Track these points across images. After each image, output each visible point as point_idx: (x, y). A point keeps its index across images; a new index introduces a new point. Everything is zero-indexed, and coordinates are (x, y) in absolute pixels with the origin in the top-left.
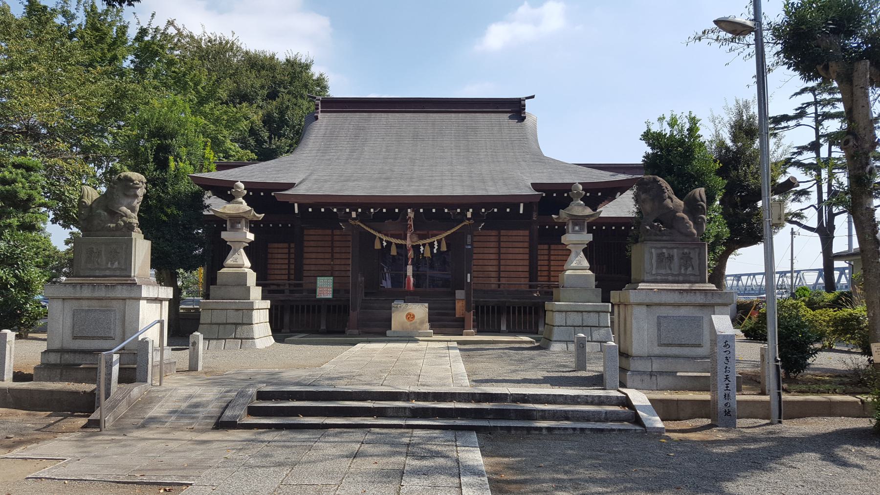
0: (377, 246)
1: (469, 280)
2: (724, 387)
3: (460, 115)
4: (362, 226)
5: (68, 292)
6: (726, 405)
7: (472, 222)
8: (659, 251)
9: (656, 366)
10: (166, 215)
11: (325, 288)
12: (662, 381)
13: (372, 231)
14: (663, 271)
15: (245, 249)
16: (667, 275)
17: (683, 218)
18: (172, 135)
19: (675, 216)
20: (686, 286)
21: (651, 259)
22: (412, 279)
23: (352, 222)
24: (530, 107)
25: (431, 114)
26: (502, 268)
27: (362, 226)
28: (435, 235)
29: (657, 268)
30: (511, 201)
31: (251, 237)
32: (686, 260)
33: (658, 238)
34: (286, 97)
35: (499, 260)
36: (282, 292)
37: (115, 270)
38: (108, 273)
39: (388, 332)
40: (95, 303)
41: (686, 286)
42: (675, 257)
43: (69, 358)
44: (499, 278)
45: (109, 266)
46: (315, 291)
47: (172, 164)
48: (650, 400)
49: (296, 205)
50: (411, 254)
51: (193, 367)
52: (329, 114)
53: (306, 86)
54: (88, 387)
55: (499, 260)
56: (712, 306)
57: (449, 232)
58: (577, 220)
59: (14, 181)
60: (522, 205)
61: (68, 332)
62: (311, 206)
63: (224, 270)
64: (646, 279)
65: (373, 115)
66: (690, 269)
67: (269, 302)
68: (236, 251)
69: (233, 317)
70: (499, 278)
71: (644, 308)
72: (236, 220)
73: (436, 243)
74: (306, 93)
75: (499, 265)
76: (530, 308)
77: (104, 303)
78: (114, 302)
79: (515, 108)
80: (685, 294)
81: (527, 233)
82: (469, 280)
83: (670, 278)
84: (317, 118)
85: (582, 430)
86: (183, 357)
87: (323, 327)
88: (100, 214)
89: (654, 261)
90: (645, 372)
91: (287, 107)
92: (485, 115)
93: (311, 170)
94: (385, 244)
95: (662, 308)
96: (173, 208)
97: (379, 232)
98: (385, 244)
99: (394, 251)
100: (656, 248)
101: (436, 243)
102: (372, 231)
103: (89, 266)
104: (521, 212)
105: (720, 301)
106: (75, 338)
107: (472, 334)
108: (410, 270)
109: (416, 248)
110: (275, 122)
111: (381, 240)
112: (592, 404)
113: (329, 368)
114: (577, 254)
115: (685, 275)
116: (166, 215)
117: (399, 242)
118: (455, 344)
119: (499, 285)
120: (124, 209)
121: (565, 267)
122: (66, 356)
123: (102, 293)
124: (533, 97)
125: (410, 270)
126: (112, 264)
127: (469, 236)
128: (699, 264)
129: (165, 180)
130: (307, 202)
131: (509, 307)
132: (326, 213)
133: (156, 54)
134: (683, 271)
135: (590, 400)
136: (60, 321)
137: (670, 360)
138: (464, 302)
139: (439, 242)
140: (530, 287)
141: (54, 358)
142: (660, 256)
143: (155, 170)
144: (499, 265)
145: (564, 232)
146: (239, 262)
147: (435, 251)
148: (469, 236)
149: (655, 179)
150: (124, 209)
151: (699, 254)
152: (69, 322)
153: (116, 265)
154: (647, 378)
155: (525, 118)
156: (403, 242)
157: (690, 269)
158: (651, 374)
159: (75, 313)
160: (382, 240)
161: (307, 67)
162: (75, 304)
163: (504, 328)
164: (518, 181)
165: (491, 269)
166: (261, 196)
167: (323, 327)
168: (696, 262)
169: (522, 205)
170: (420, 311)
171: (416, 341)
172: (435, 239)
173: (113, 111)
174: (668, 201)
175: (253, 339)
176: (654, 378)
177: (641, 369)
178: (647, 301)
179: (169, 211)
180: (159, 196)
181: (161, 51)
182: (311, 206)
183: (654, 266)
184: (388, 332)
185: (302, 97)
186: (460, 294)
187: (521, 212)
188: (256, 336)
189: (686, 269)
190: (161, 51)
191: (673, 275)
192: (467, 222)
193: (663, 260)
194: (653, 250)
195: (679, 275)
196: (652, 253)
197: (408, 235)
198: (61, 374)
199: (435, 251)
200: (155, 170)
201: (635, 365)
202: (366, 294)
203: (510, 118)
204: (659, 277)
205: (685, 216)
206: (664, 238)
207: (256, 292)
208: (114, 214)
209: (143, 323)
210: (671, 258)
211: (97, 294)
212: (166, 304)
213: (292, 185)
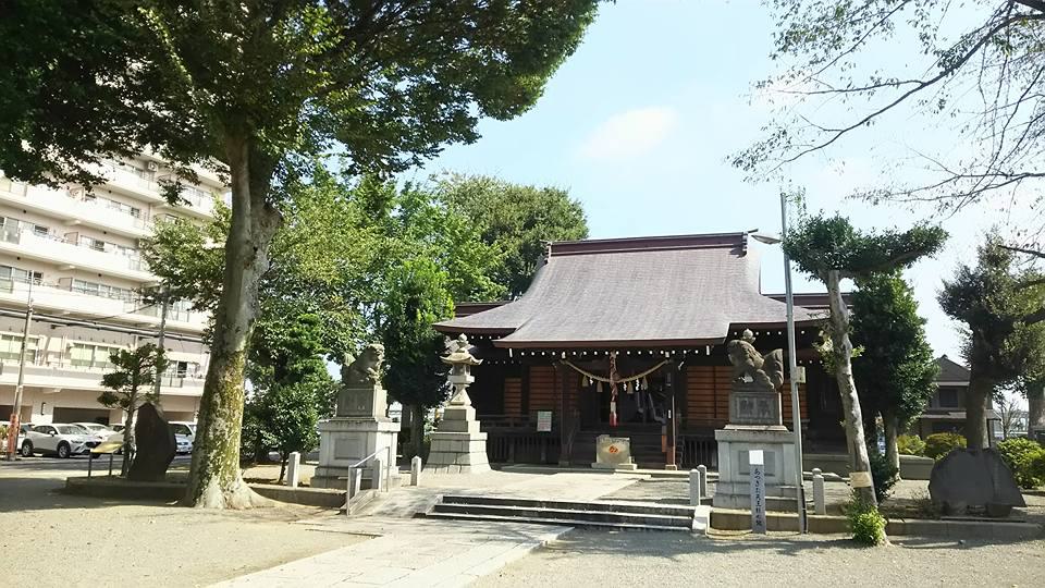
0: (585, 384)
2: (756, 503)
3: (682, 251)
5: (333, 427)
9: (736, 490)
10: (414, 357)
11: (544, 422)
12: (740, 501)
14: (746, 416)
15: (466, 389)
18: (421, 290)
20: (763, 428)
28: (637, 374)
30: (699, 344)
31: (471, 379)
32: (763, 406)
34: (542, 227)
36: (508, 425)
38: (358, 413)
40: (350, 434)
41: (763, 428)
42: (755, 405)
43: (333, 472)
44: (715, 414)
47: (419, 315)
50: (614, 391)
51: (414, 483)
54: (342, 492)
56: (781, 443)
57: (650, 371)
59: (300, 334)
62: (524, 350)
67: (485, 434)
69: (455, 446)
70: (715, 414)
77: (355, 434)
78: (361, 434)
83: (751, 421)
84: (546, 262)
85: (647, 529)
86: (407, 477)
87: (543, 458)
90: (726, 495)
93: (531, 320)
94: (592, 382)
96: (420, 353)
98: (592, 382)
105: (786, 440)
106: (337, 458)
107: (674, 469)
108: (613, 406)
109: (620, 386)
110: (530, 251)
113: (505, 488)
116: (414, 357)
117: (604, 380)
122: (330, 470)
125: (613, 406)
129: (414, 328)
130: (519, 347)
132: (541, 355)
133: (418, 205)
134: (761, 415)
136: (327, 450)
139: (641, 380)
141: (323, 472)
142: (743, 404)
144: (715, 401)
147: (637, 388)
152: (333, 447)
153: (766, 415)
154: (728, 499)
155: (745, 253)
159: (337, 441)
161: (564, 195)
162: (337, 434)
165: (707, 404)
166: (484, 341)
167: (543, 458)
168: (771, 408)
170: (622, 446)
173: (377, 265)
178: (728, 439)
181: (422, 202)
182: (524, 350)
190: (422, 202)
192: (666, 362)
194: (738, 399)
195: (758, 418)
199: (637, 388)
203: (732, 253)
207: (474, 426)
208: (365, 373)
209: (379, 446)
210: (751, 405)
211: (351, 428)
212: (396, 435)
213: (512, 330)
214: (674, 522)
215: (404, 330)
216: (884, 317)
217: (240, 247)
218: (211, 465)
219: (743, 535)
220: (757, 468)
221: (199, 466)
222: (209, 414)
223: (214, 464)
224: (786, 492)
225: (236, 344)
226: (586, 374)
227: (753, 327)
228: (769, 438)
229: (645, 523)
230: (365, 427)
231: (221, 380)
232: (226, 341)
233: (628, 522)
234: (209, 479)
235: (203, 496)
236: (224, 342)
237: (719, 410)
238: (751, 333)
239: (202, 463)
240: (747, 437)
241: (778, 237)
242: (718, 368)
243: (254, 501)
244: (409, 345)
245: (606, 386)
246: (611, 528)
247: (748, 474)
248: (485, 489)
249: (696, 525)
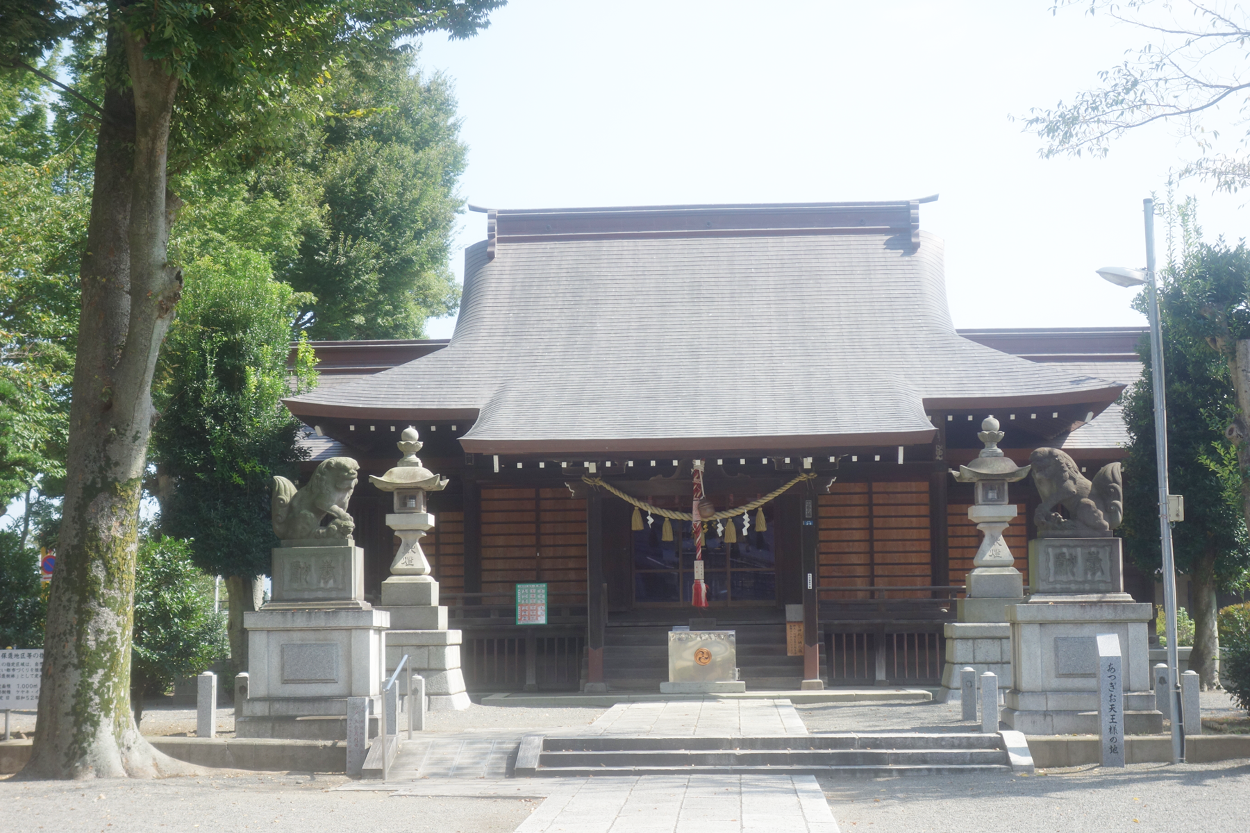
0: (637, 524)
1: (810, 586)
2: (1108, 719)
3: (786, 239)
4: (608, 488)
6: (1111, 740)
7: (813, 475)
8: (1058, 551)
9: (1053, 703)
10: (242, 474)
12: (1059, 721)
13: (626, 498)
14: (1064, 578)
16: (1069, 582)
17: (1089, 506)
19: (1079, 503)
21: (1048, 560)
22: (703, 586)
23: (589, 482)
24: (926, 219)
25: (725, 240)
26: (878, 558)
27: (608, 488)
28: (745, 503)
29: (1056, 573)
30: (883, 445)
32: (1093, 562)
33: (1057, 532)
35: (871, 541)
37: (331, 590)
38: (320, 594)
39: (663, 686)
40: (310, 637)
41: (1094, 597)
42: (1080, 560)
43: (281, 709)
44: (872, 578)
45: (322, 585)
46: (513, 612)
47: (253, 381)
48: (1028, 742)
49: (496, 459)
50: (700, 539)
52: (514, 246)
53: (406, 112)
55: (871, 541)
57: (770, 497)
58: (991, 481)
60: (901, 450)
61: (275, 674)
62: (591, 457)
63: (391, 580)
64: (1041, 588)
65: (606, 243)
66: (1099, 574)
68: (409, 546)
70: (872, 578)
71: (1036, 628)
72: (408, 493)
73: (746, 517)
74: (406, 128)
75: (871, 553)
76: (911, 636)
77: (321, 635)
78: (336, 634)
79: (896, 225)
80: (1088, 608)
81: (924, 486)
82: (810, 586)
83: (1073, 587)
85: (939, 770)
88: (305, 516)
89: (1051, 564)
90: (1037, 712)
91: (372, 171)
92: (836, 238)
94: (651, 520)
95: (1061, 627)
97: (640, 499)
98: (651, 520)
99: (668, 535)
100: (1053, 547)
101: (746, 517)
102: (626, 498)
103: (295, 586)
104: (901, 461)
105: (1133, 616)
106: (286, 682)
107: (817, 687)
108: (699, 569)
111: (644, 514)
112: (959, 747)
114: (994, 540)
115: (1093, 582)
116: (242, 474)
117: (677, 516)
118: (788, 702)
119: (872, 593)
120: (336, 507)
121: (976, 562)
122: (277, 706)
123: (321, 622)
124: (934, 198)
125: (699, 569)
126: (326, 582)
127: (808, 504)
128: (1111, 568)
130: (513, 453)
131: (890, 636)
134: (1089, 577)
135: (957, 742)
137: (1071, 695)
138: (802, 627)
139: (752, 514)
140: (935, 594)
142: (1059, 557)
143: (219, 391)
144: (871, 553)
145: (972, 502)
146: (417, 566)
147: (745, 533)
148: (808, 504)
149: (1051, 453)
150: (336, 507)
151: (1111, 553)
152: (276, 660)
153: (331, 583)
154: (1039, 719)
156: (685, 517)
157: (1099, 574)
158: (1046, 714)
160: (644, 513)
162: (284, 638)
163: (881, 675)
164: (887, 402)
165: (855, 559)
169: (901, 450)
171: (715, 698)
172: (744, 509)
174: (1070, 482)
175: (448, 694)
176: (1049, 719)
177: (1033, 707)
178: (1039, 618)
179: (248, 467)
180: (229, 440)
183: (1052, 571)
184: (663, 686)
185: (402, 140)
186: (794, 612)
187: (901, 461)
188: (451, 691)
189: (1094, 574)
191: (1076, 582)
192: (803, 477)
193: (1063, 562)
194: (1050, 550)
196: (1048, 554)
197: (695, 504)
198: (273, 728)
199: (745, 533)
200: (219, 391)
201: (1026, 703)
202: (612, 614)
203: (889, 245)
204: (1058, 586)
205: (1092, 503)
206: (1066, 532)
210: (1073, 560)
214: (973, 759)
215: (214, 411)
216: (1207, 387)
217: (150, 275)
218: (97, 700)
219: (1079, 772)
220: (1111, 664)
221: (73, 701)
222: (84, 600)
223: (101, 695)
224: (1133, 703)
225: (127, 461)
226: (637, 504)
227: (422, 419)
228: (1108, 614)
229: (925, 762)
230: (344, 620)
231: (103, 535)
232: (114, 459)
233: (897, 762)
234: (96, 724)
235: (88, 758)
236: (108, 459)
237: (879, 570)
238: (996, 423)
239: (78, 694)
240: (1076, 613)
241: (1139, 276)
242: (877, 487)
243: (162, 766)
244: (229, 446)
245: (684, 530)
246: (877, 773)
247: (1093, 675)
248: (530, 729)
249: (1015, 759)
